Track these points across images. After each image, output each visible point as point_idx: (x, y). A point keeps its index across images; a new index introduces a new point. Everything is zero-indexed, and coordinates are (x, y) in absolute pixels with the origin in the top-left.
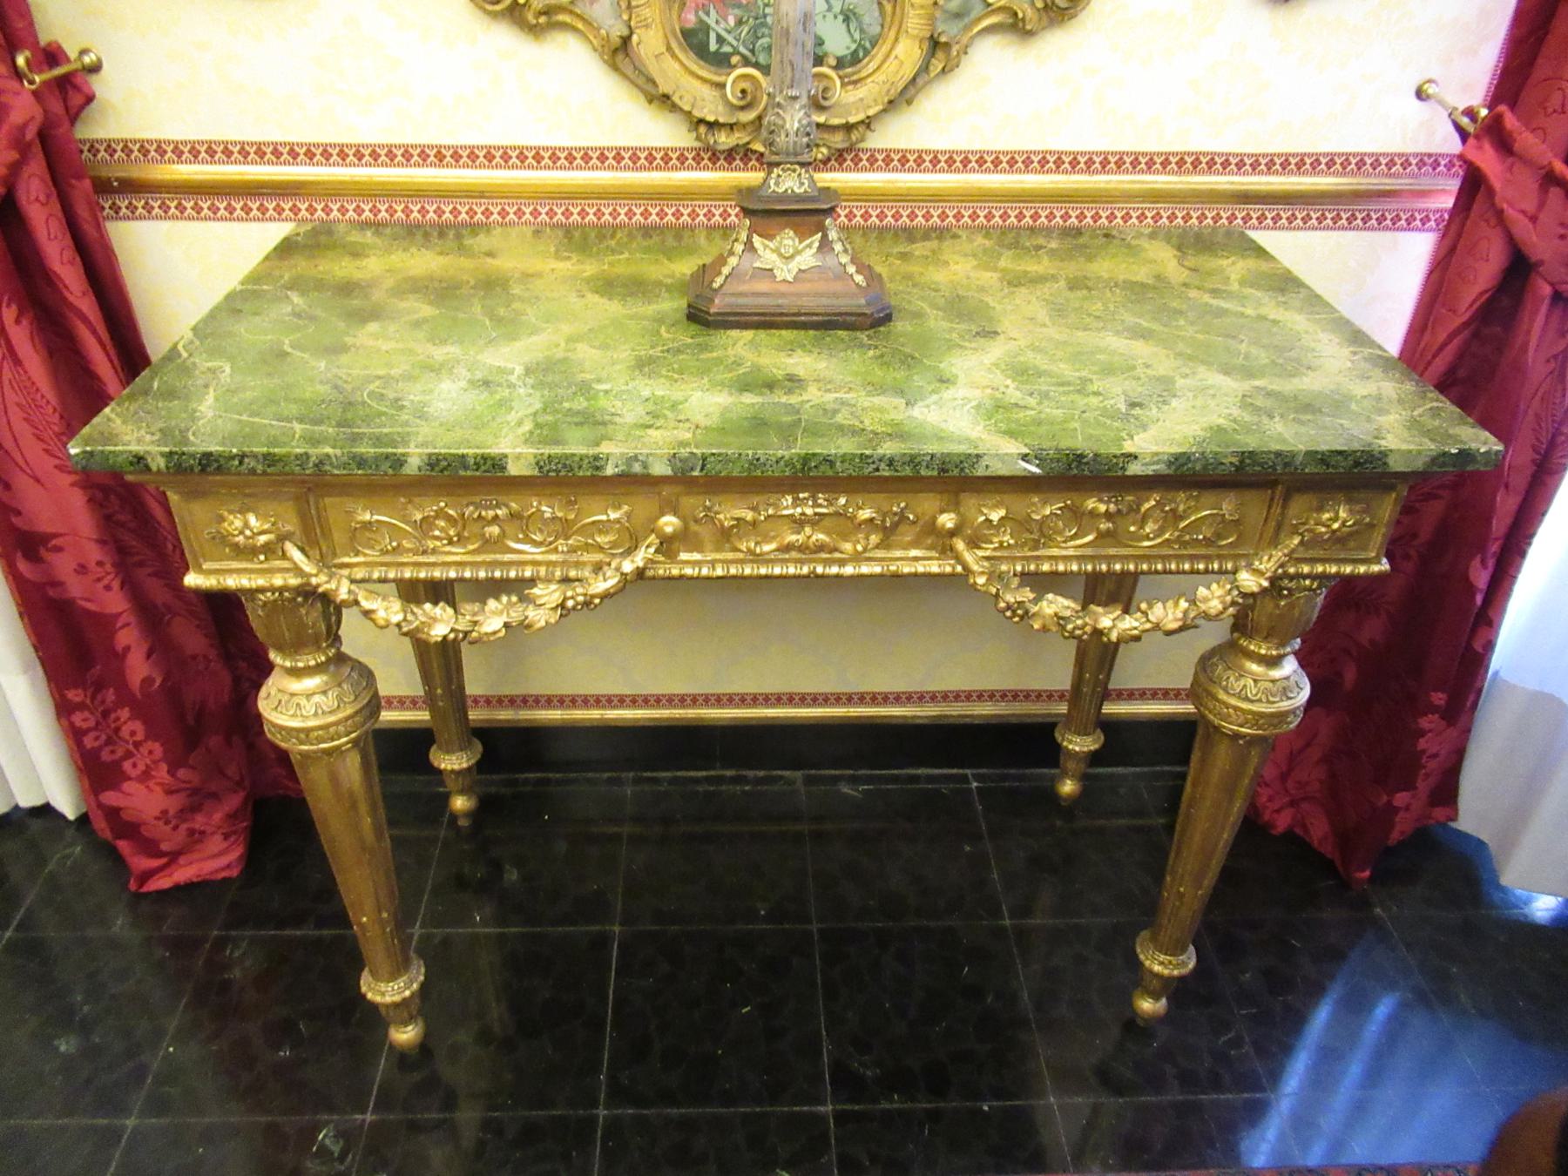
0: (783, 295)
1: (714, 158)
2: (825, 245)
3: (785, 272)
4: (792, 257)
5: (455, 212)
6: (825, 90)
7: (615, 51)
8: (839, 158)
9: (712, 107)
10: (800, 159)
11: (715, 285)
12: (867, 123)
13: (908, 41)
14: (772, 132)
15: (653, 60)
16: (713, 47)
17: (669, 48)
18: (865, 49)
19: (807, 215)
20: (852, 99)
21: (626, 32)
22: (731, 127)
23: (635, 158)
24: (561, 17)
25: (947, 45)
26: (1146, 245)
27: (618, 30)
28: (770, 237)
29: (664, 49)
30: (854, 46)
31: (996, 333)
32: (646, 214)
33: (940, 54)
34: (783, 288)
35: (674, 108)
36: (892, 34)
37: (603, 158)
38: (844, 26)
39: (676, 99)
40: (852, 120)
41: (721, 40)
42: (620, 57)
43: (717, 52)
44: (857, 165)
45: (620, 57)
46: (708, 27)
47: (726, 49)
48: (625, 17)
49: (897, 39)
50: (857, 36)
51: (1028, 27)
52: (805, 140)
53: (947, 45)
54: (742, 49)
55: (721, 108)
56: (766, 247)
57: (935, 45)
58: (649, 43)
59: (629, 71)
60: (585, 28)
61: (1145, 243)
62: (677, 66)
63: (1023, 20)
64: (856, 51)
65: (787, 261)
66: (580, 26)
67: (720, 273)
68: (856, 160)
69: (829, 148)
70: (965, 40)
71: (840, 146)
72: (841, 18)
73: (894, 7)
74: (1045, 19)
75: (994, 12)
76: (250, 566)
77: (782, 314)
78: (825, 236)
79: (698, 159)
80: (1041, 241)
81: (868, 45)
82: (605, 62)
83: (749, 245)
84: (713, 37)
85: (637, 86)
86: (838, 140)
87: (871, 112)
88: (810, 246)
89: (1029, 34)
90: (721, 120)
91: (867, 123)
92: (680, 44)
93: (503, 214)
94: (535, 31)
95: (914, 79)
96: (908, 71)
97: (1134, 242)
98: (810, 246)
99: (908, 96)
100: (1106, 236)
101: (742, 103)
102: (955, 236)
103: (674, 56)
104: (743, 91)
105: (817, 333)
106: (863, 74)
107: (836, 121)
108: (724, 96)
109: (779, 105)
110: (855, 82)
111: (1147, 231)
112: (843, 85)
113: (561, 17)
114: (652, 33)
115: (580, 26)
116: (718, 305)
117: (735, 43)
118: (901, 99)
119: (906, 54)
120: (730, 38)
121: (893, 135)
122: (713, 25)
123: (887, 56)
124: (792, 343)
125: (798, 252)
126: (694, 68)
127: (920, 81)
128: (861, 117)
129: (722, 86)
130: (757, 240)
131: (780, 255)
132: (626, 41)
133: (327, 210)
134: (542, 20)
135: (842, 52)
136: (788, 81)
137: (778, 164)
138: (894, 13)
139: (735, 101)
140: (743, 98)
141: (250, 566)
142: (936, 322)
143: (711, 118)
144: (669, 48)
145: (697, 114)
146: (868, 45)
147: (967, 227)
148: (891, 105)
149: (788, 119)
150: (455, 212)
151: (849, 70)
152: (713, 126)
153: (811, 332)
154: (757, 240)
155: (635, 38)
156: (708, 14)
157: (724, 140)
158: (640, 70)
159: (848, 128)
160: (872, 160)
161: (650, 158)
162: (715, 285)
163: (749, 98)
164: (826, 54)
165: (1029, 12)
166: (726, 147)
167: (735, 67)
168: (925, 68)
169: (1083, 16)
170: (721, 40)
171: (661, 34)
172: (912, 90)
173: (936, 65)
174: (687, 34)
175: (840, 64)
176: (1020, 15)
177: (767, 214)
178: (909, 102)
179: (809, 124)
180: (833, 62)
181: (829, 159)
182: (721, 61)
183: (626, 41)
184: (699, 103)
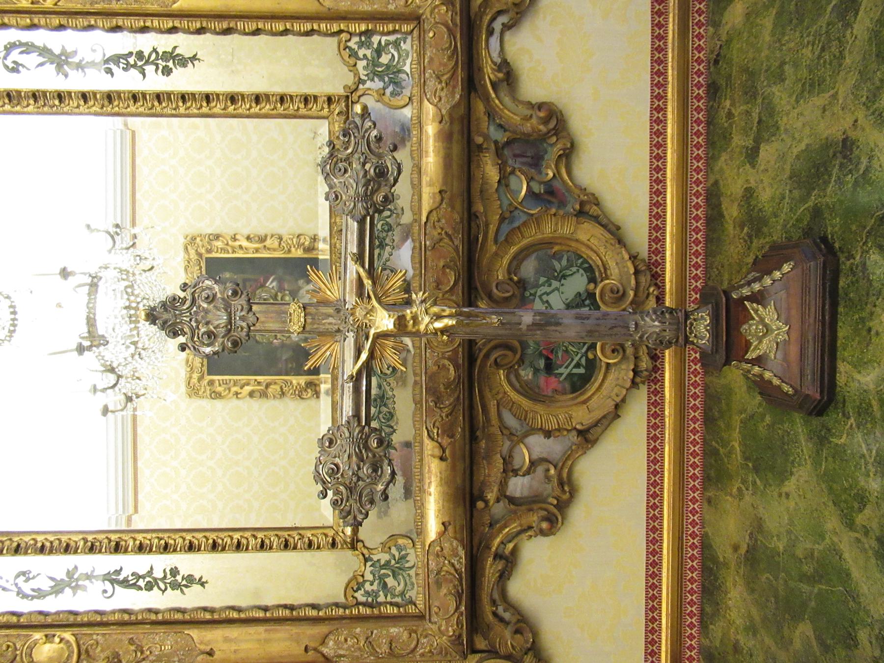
0: (803, 335)
1: (655, 369)
2: (758, 298)
3: (779, 329)
4: (766, 326)
5: (692, 558)
6: (612, 291)
7: (587, 440)
8: (657, 278)
9: (623, 372)
10: (682, 320)
11: (791, 391)
12: (633, 258)
13: (579, 232)
14: (661, 342)
15: (592, 414)
16: (582, 371)
17: (584, 402)
18: (582, 263)
19: (730, 316)
20: (617, 271)
21: (574, 433)
22: (636, 358)
23: (655, 427)
24: (565, 475)
25: (582, 204)
26: (727, 28)
27: (573, 437)
28: (748, 344)
29: (585, 406)
30: (581, 271)
31: (844, 141)
32: (694, 420)
33: (587, 208)
34: (795, 335)
35: (623, 400)
36: (573, 244)
37: (655, 450)
38: (568, 279)
39: (618, 399)
40: (632, 271)
41: (578, 365)
42: (590, 436)
43: (586, 368)
44: (661, 264)
45: (590, 436)
46: (570, 375)
47: (583, 361)
48: (565, 433)
49: (577, 241)
50: (574, 269)
51: (569, 145)
52: (667, 316)
53: (582, 204)
54: (584, 350)
55: (623, 367)
56: (756, 348)
57: (581, 213)
58: (581, 416)
59: (599, 429)
60: (569, 459)
61: (723, 32)
62: (596, 397)
63: (564, 150)
64: (584, 269)
65: (772, 331)
66: (570, 463)
67: (779, 387)
68: (657, 264)
69: (650, 286)
70: (577, 191)
71: (649, 277)
72: (563, 281)
73: (557, 244)
74: (564, 134)
75: (559, 172)
76: (507, 310)
77: (823, 336)
78: (748, 298)
79: (656, 381)
80: (723, 114)
81: (580, 261)
82: (592, 447)
83: (758, 361)
84: (575, 371)
85: (609, 425)
86: (645, 279)
87: (627, 257)
88: (756, 311)
89: (573, 145)
90: (632, 367)
91: (633, 258)
92: (581, 394)
93: (694, 524)
94: (573, 492)
95: (602, 226)
96: (599, 231)
97: (724, 37)
98: (756, 311)
99: (614, 229)
100: (716, 62)
101: (621, 351)
102: (716, 183)
103: (589, 398)
104: (613, 351)
105: (842, 303)
106: (600, 263)
107: (633, 282)
108: (615, 364)
109: (641, 337)
110: (605, 269)
111: (711, 30)
112: (607, 278)
113: (565, 475)
114: (574, 415)
115: (570, 463)
116: (813, 391)
117: (579, 355)
118: (615, 233)
119: (588, 234)
120: (576, 359)
121: (638, 233)
122: (568, 370)
123: (588, 247)
124: (856, 331)
125: (762, 320)
126: (597, 385)
127: (605, 221)
128: (630, 264)
129: (608, 364)
130: (750, 355)
131: (764, 335)
132: (580, 433)
133: (691, 648)
134: (566, 488)
135: (585, 280)
136: (623, 331)
137: (686, 338)
138: (560, 244)
139: (620, 357)
140: (618, 352)
141: (507, 310)
142: (830, 194)
143: (631, 374)
144: (584, 402)
145: (628, 384)
146: (580, 261)
147: (706, 177)
148: (621, 242)
149: (651, 330)
150: (692, 558)
151: (597, 274)
152: (636, 372)
153: (841, 309)
154: (750, 355)
155: (578, 427)
156: (562, 374)
157: (645, 363)
158: (596, 424)
159: (637, 272)
160: (657, 252)
161: (655, 415)
162: (791, 391)
163: (618, 347)
164: (587, 290)
165: (559, 146)
166: (650, 362)
167: (595, 356)
168: (596, 219)
169: (560, 107)
170: (578, 365)
171: (574, 408)
172: (610, 226)
173: (594, 210)
174: (574, 389)
175: (592, 280)
176: (561, 152)
177: (729, 344)
178: (618, 228)
179: (655, 312)
180: (592, 286)
181: (656, 285)
182: (591, 365)
183: (580, 433)
184: (620, 382)
